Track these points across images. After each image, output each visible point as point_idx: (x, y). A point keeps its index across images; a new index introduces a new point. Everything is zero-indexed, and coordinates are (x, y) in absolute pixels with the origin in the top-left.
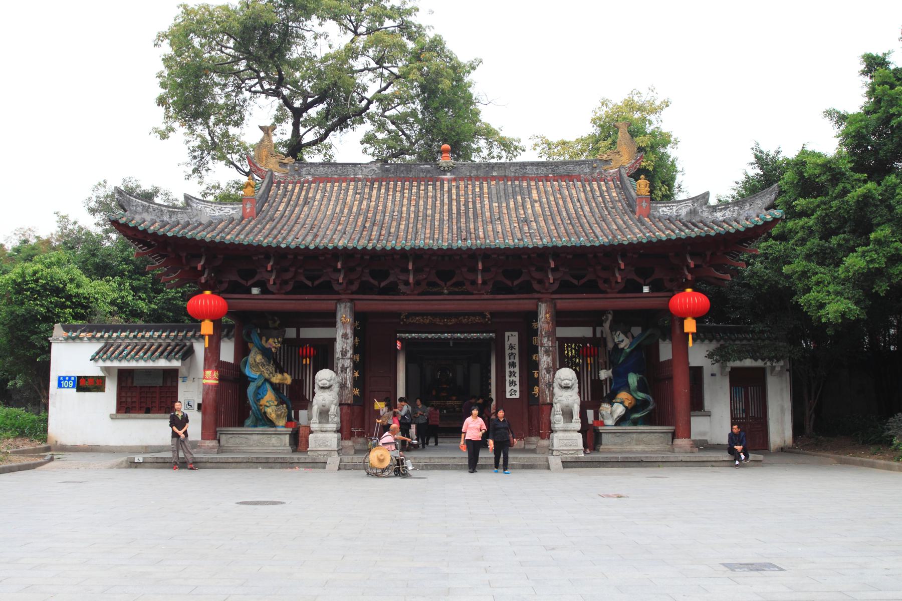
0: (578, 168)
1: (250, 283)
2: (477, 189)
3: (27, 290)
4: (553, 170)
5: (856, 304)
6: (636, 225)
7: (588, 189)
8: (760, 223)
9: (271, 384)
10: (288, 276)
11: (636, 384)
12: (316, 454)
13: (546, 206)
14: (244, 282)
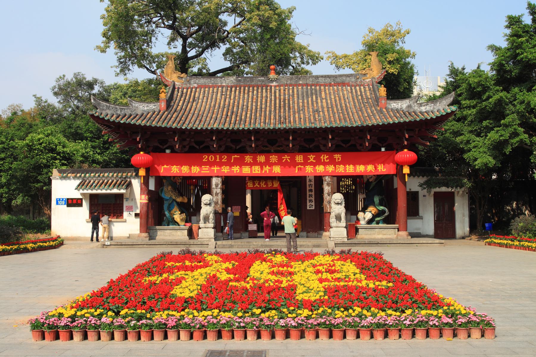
0: (348, 78)
1: (165, 147)
2: (291, 91)
3: (35, 150)
4: (334, 80)
5: (494, 158)
6: (378, 114)
7: (354, 91)
8: (444, 114)
9: (176, 202)
10: (185, 143)
11: (378, 201)
12: (203, 240)
13: (329, 102)
14: (161, 147)
